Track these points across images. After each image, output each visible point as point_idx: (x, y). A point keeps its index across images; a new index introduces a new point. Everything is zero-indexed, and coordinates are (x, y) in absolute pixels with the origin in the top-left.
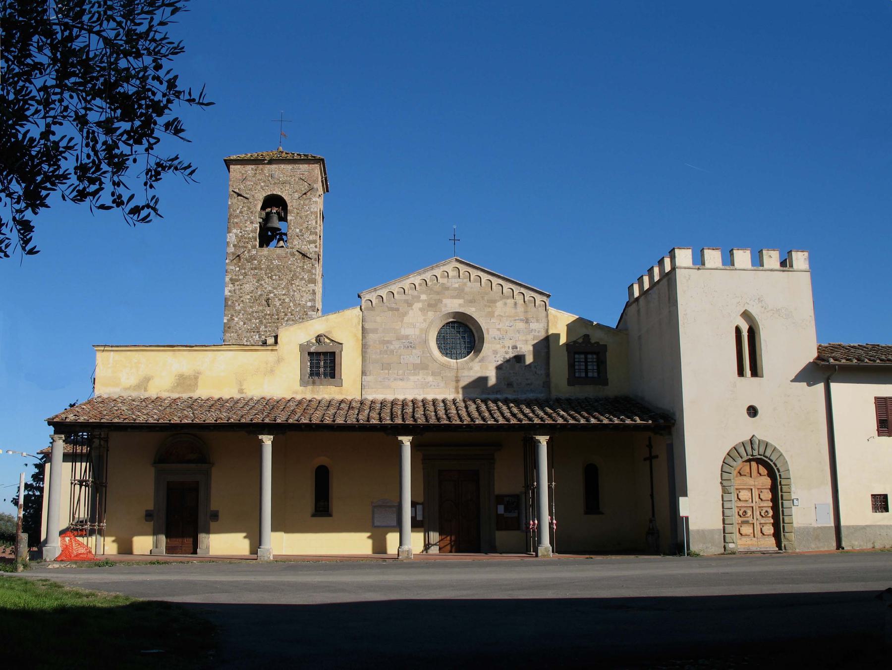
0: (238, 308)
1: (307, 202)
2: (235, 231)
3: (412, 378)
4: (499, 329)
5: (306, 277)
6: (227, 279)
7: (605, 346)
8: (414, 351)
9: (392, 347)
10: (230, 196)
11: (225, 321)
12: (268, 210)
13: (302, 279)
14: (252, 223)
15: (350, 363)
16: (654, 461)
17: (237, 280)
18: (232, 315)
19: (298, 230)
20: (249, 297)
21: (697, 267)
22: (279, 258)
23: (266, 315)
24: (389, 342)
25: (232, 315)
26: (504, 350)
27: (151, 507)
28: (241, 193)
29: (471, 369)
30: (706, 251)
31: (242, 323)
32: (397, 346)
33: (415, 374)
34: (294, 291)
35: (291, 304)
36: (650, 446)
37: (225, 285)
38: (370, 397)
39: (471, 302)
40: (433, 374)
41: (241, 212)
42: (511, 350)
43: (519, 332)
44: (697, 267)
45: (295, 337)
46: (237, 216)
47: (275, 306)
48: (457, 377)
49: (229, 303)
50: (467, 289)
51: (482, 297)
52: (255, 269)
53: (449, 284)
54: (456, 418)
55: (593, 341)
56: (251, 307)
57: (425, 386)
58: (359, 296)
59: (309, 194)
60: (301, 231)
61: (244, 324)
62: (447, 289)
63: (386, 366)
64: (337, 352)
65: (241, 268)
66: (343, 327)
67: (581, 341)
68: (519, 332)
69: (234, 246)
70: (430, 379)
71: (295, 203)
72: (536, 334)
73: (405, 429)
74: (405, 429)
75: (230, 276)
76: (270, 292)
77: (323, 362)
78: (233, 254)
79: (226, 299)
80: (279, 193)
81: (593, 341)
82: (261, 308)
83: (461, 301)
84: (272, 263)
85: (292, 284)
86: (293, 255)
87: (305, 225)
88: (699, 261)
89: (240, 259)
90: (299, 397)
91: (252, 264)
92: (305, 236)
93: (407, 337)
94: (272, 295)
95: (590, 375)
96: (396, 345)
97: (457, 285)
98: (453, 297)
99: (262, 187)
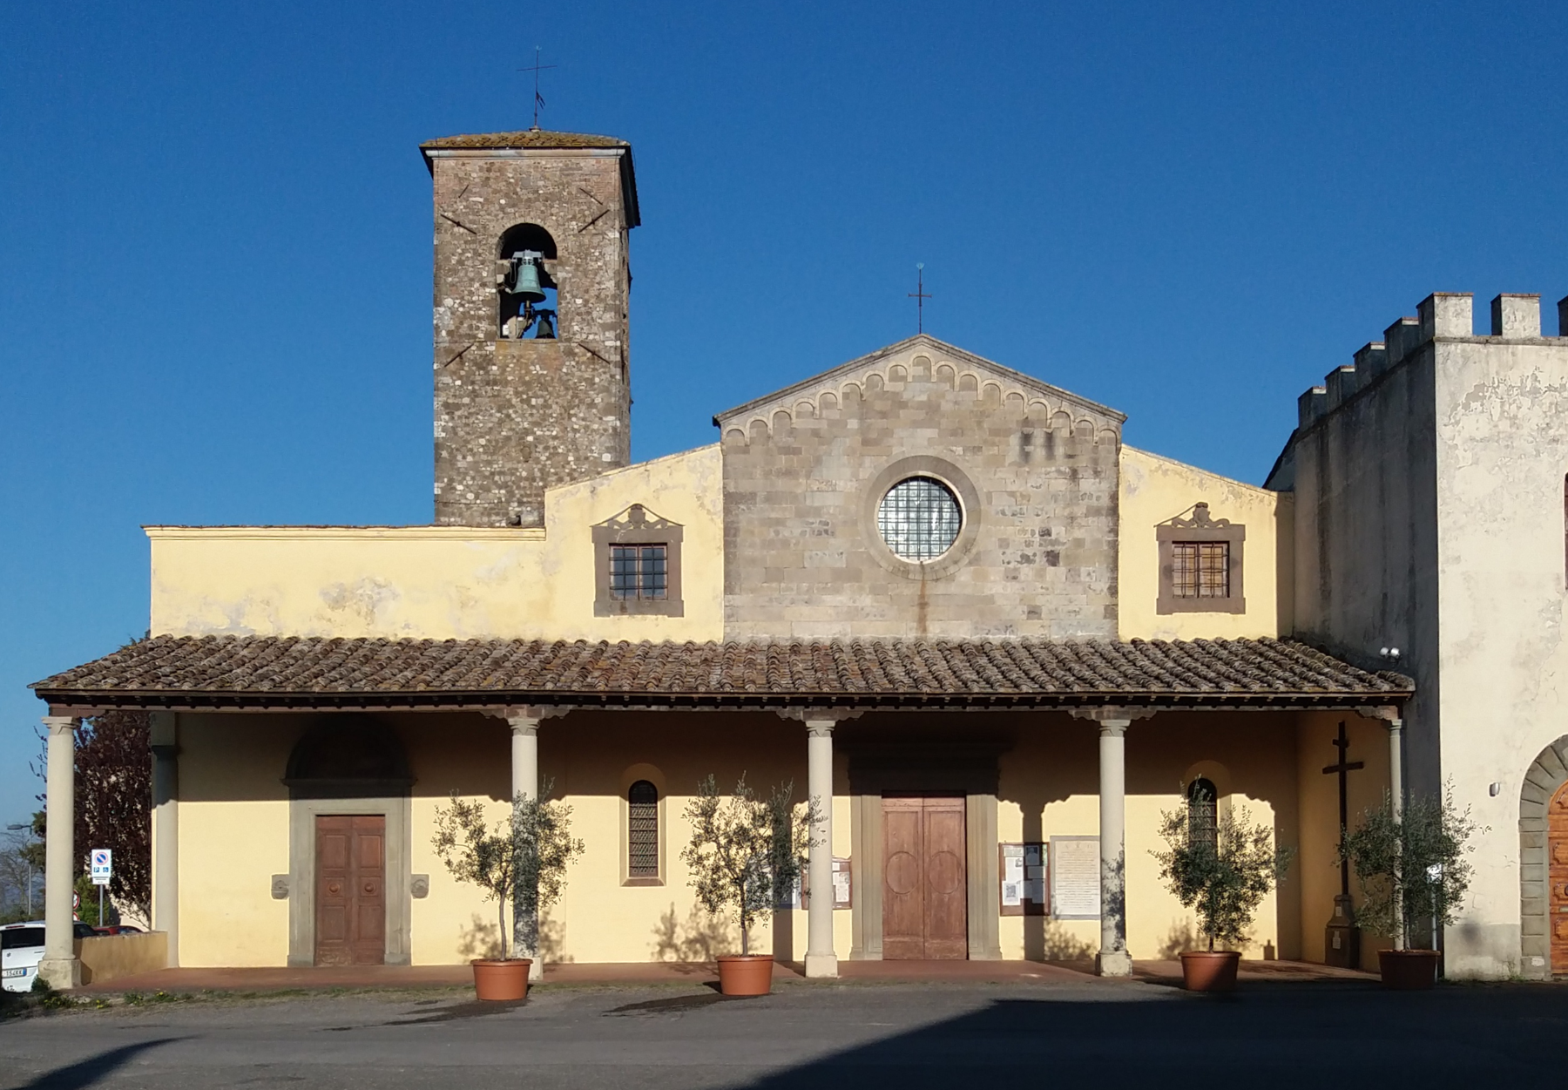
0: (461, 464)
1: (596, 240)
2: (448, 302)
3: (828, 598)
4: (1012, 494)
5: (598, 400)
6: (437, 403)
7: (1241, 528)
8: (832, 541)
9: (785, 533)
10: (438, 228)
11: (437, 491)
12: (517, 254)
13: (592, 405)
14: (484, 285)
15: (700, 567)
16: (1352, 775)
17: (458, 407)
18: (451, 480)
19: (579, 301)
20: (483, 441)
21: (1482, 338)
22: (542, 360)
23: (521, 479)
24: (779, 522)
25: (451, 480)
26: (1021, 538)
27: (285, 870)
28: (460, 219)
29: (951, 578)
30: (1506, 303)
31: (471, 496)
32: (797, 532)
33: (837, 591)
34: (575, 431)
35: (571, 458)
36: (1342, 743)
37: (431, 416)
38: (744, 639)
39: (954, 433)
40: (875, 591)
41: (460, 262)
42: (1037, 538)
43: (1055, 498)
44: (1482, 338)
45: (580, 510)
46: (454, 272)
47: (537, 461)
48: (922, 596)
49: (444, 454)
50: (946, 406)
51: (979, 423)
52: (495, 383)
53: (906, 396)
54: (952, 680)
55: (1214, 518)
56: (489, 463)
57: (853, 614)
58: (716, 423)
59: (600, 223)
60: (586, 302)
61: (477, 497)
62: (903, 405)
63: (775, 574)
64: (671, 542)
65: (468, 380)
66: (682, 490)
67: (1188, 517)
68: (1055, 498)
69: (450, 333)
70: (867, 601)
71: (571, 243)
72: (1094, 503)
73: (821, 701)
74: (821, 701)
75: (442, 398)
76: (527, 432)
77: (638, 565)
78: (448, 351)
79: (438, 446)
80: (539, 222)
81: (1214, 518)
82: (509, 465)
83: (931, 433)
84: (528, 372)
85: (570, 416)
86: (570, 353)
87: (593, 292)
88: (1492, 324)
89: (462, 363)
90: (593, 640)
91: (487, 373)
92: (595, 314)
93: (817, 511)
94: (530, 438)
95: (1202, 592)
96: (793, 530)
97: (924, 398)
98: (916, 424)
99: (502, 208)
